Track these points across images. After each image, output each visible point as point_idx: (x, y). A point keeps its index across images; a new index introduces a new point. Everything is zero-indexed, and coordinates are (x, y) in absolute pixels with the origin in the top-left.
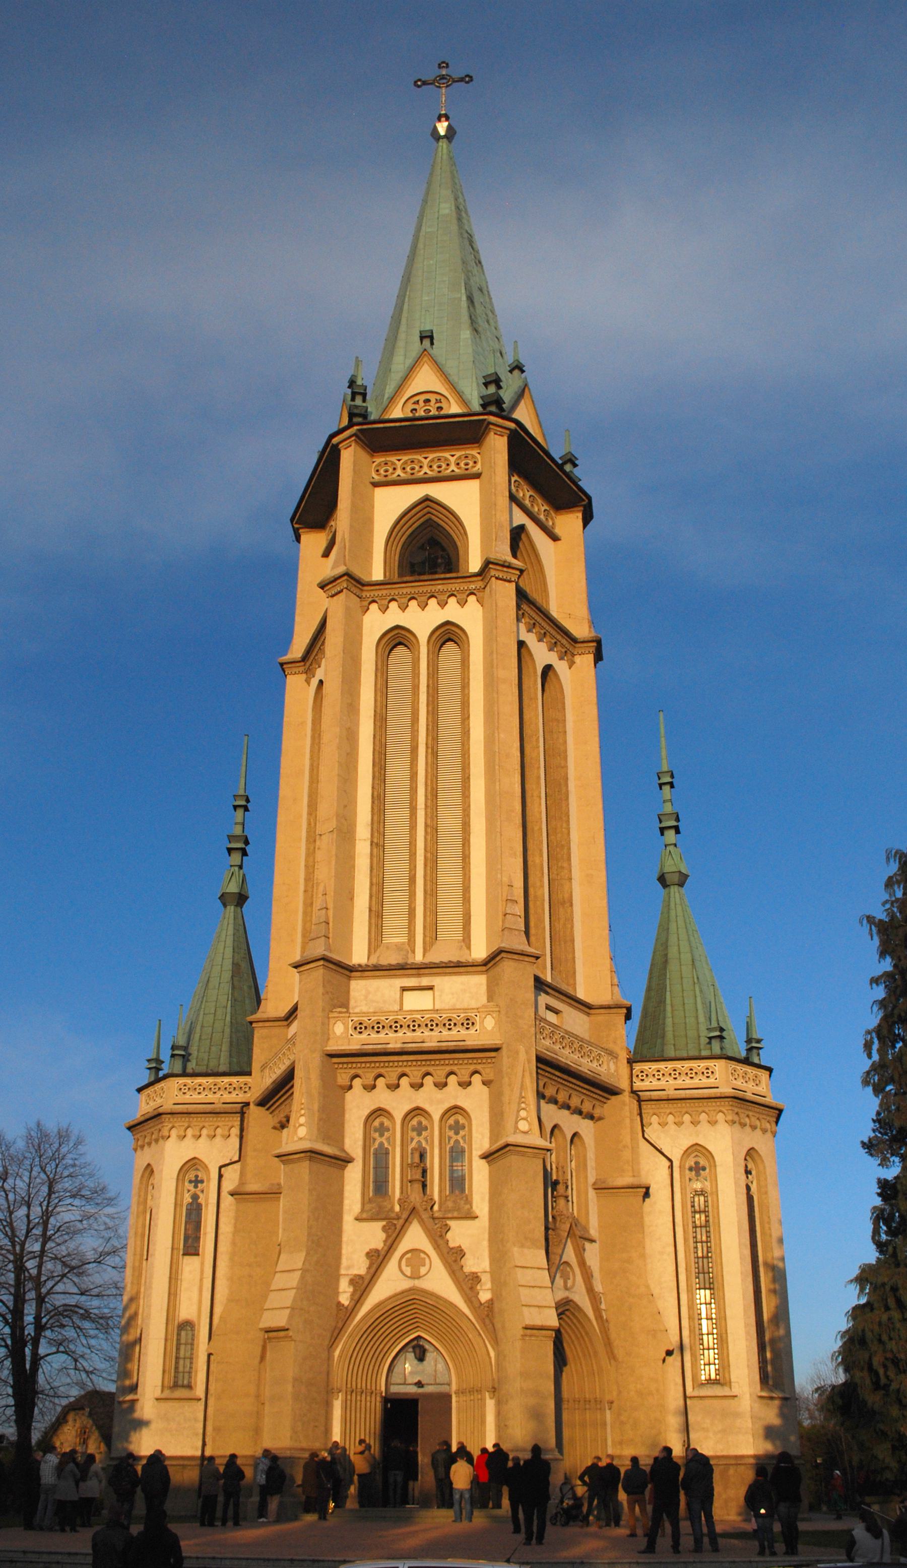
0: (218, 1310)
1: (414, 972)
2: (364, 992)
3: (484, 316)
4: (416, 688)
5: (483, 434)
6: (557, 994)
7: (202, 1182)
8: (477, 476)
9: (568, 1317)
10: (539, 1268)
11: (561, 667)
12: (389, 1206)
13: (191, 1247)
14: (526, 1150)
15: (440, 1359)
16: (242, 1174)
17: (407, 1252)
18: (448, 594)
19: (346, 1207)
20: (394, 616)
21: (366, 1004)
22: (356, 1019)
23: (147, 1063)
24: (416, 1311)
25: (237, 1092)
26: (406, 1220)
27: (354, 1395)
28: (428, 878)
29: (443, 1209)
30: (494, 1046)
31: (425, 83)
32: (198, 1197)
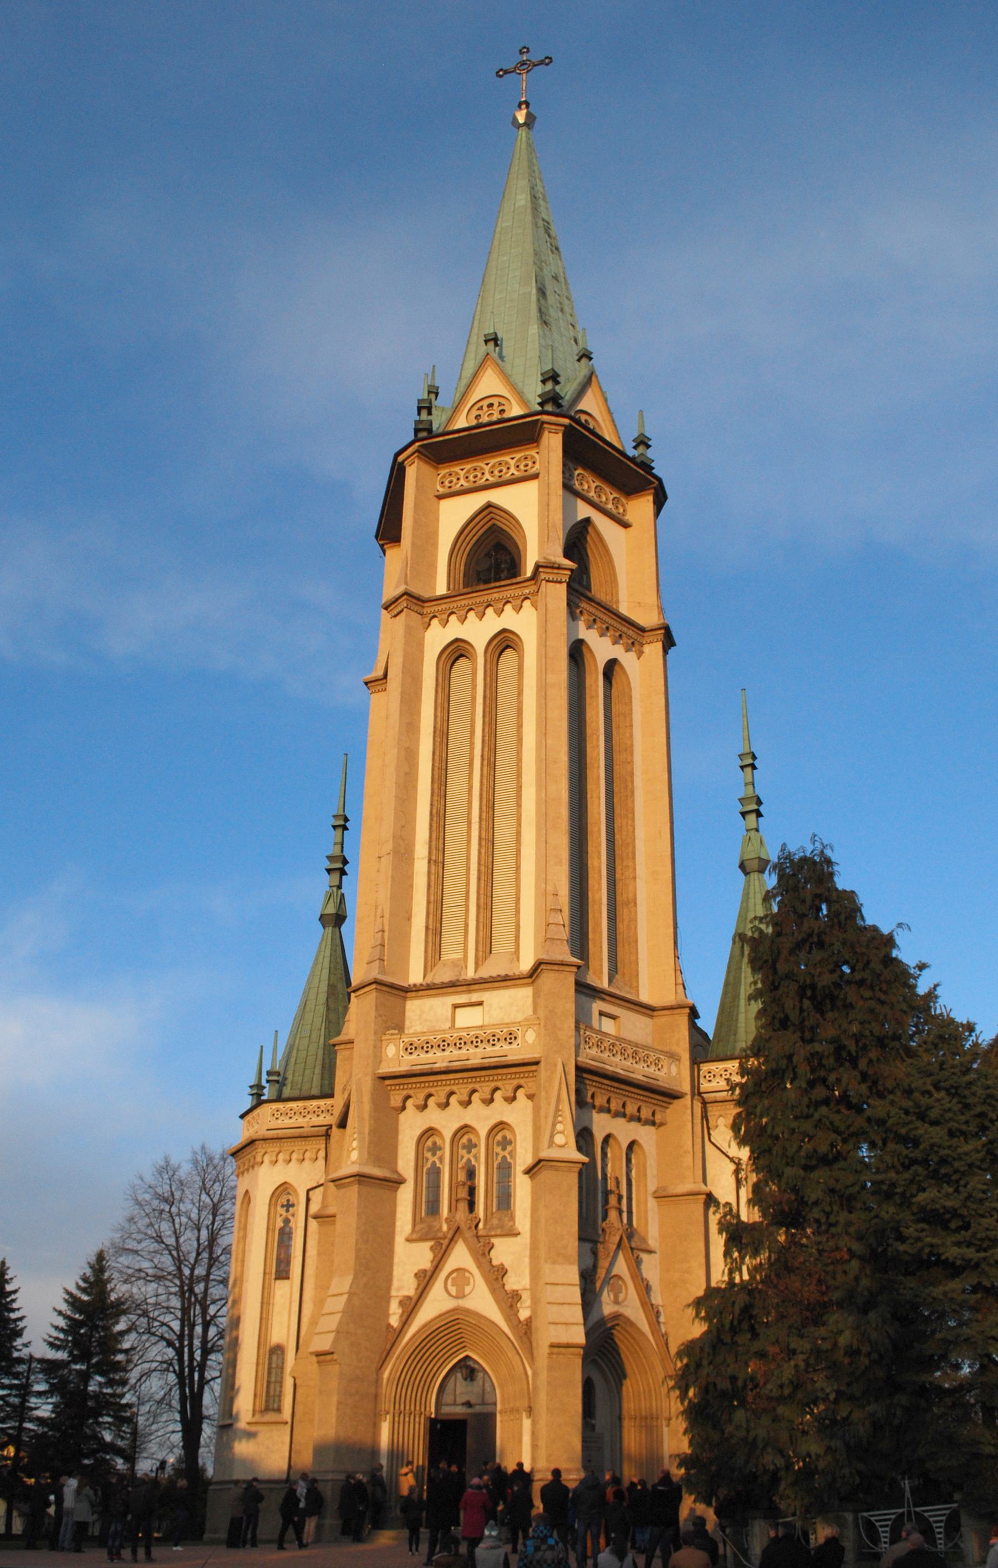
1: (464, 988)
2: (418, 1012)
3: (559, 305)
4: (474, 699)
5: (539, 434)
6: (613, 1000)
7: (293, 1205)
8: (535, 476)
9: (619, 1332)
10: (570, 1285)
11: (628, 660)
12: (438, 1227)
14: (559, 1164)
16: (324, 1198)
18: (504, 601)
19: (398, 1229)
20: (455, 629)
21: (420, 1024)
23: (249, 1090)
25: (324, 1115)
26: (451, 1240)
27: (402, 1416)
28: (482, 892)
29: (487, 1227)
30: (533, 1060)
31: (506, 72)
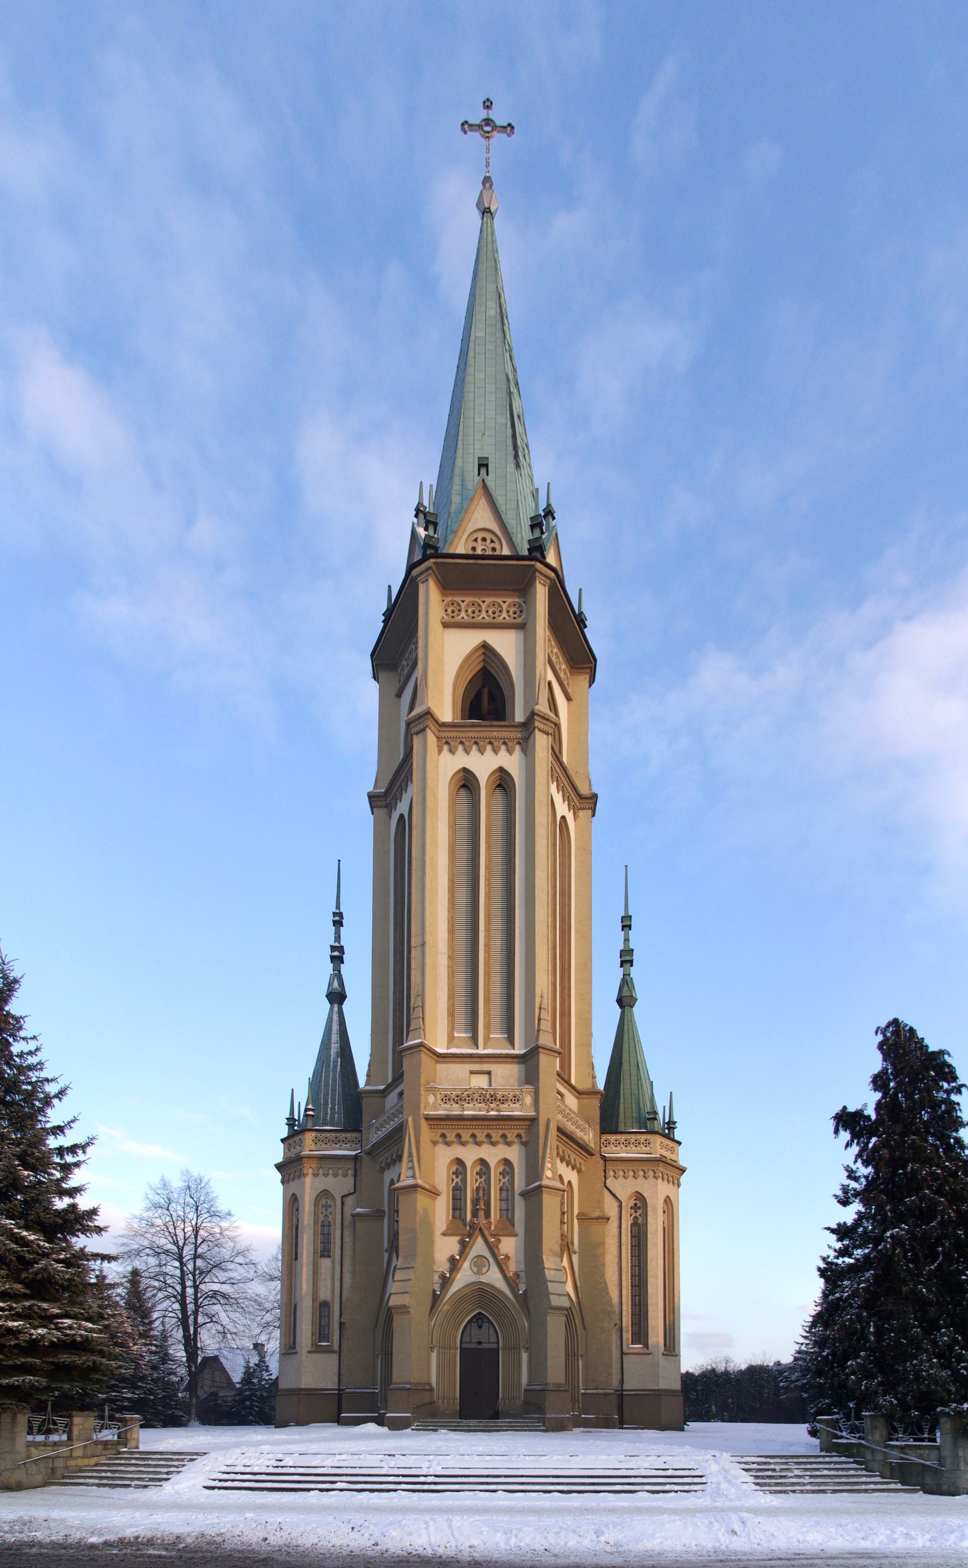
0: (345, 1293)
13: (325, 1252)
15: (491, 1327)
17: (475, 1257)
22: (443, 1093)
24: (479, 1293)
25: (341, 1144)
32: (638, 1219)
